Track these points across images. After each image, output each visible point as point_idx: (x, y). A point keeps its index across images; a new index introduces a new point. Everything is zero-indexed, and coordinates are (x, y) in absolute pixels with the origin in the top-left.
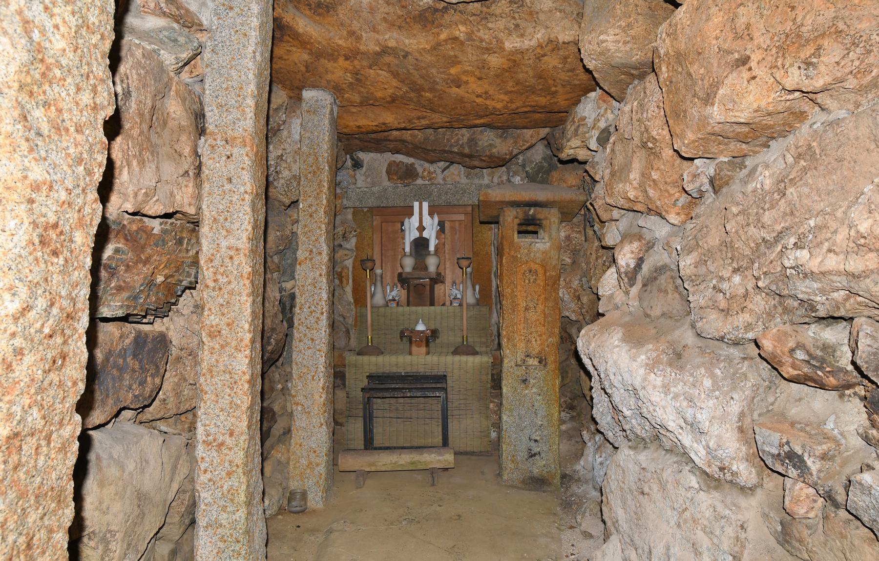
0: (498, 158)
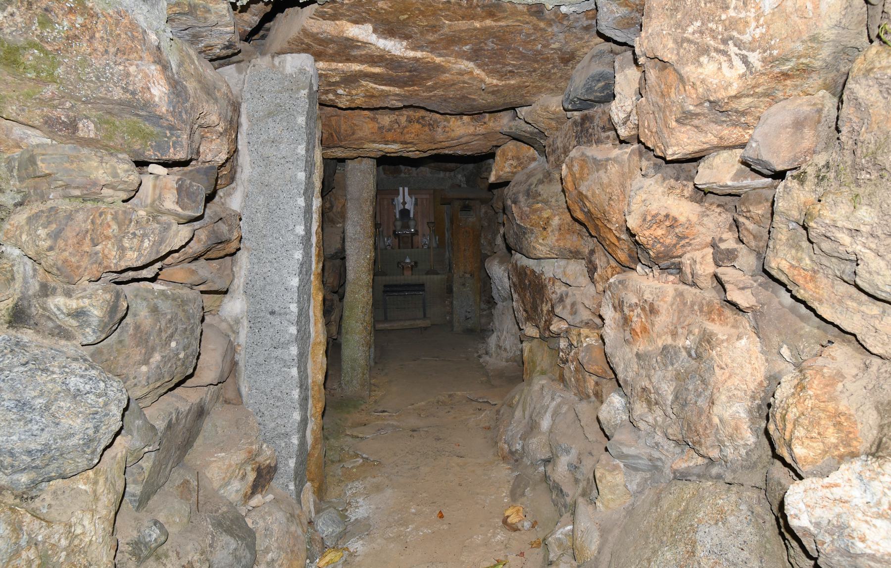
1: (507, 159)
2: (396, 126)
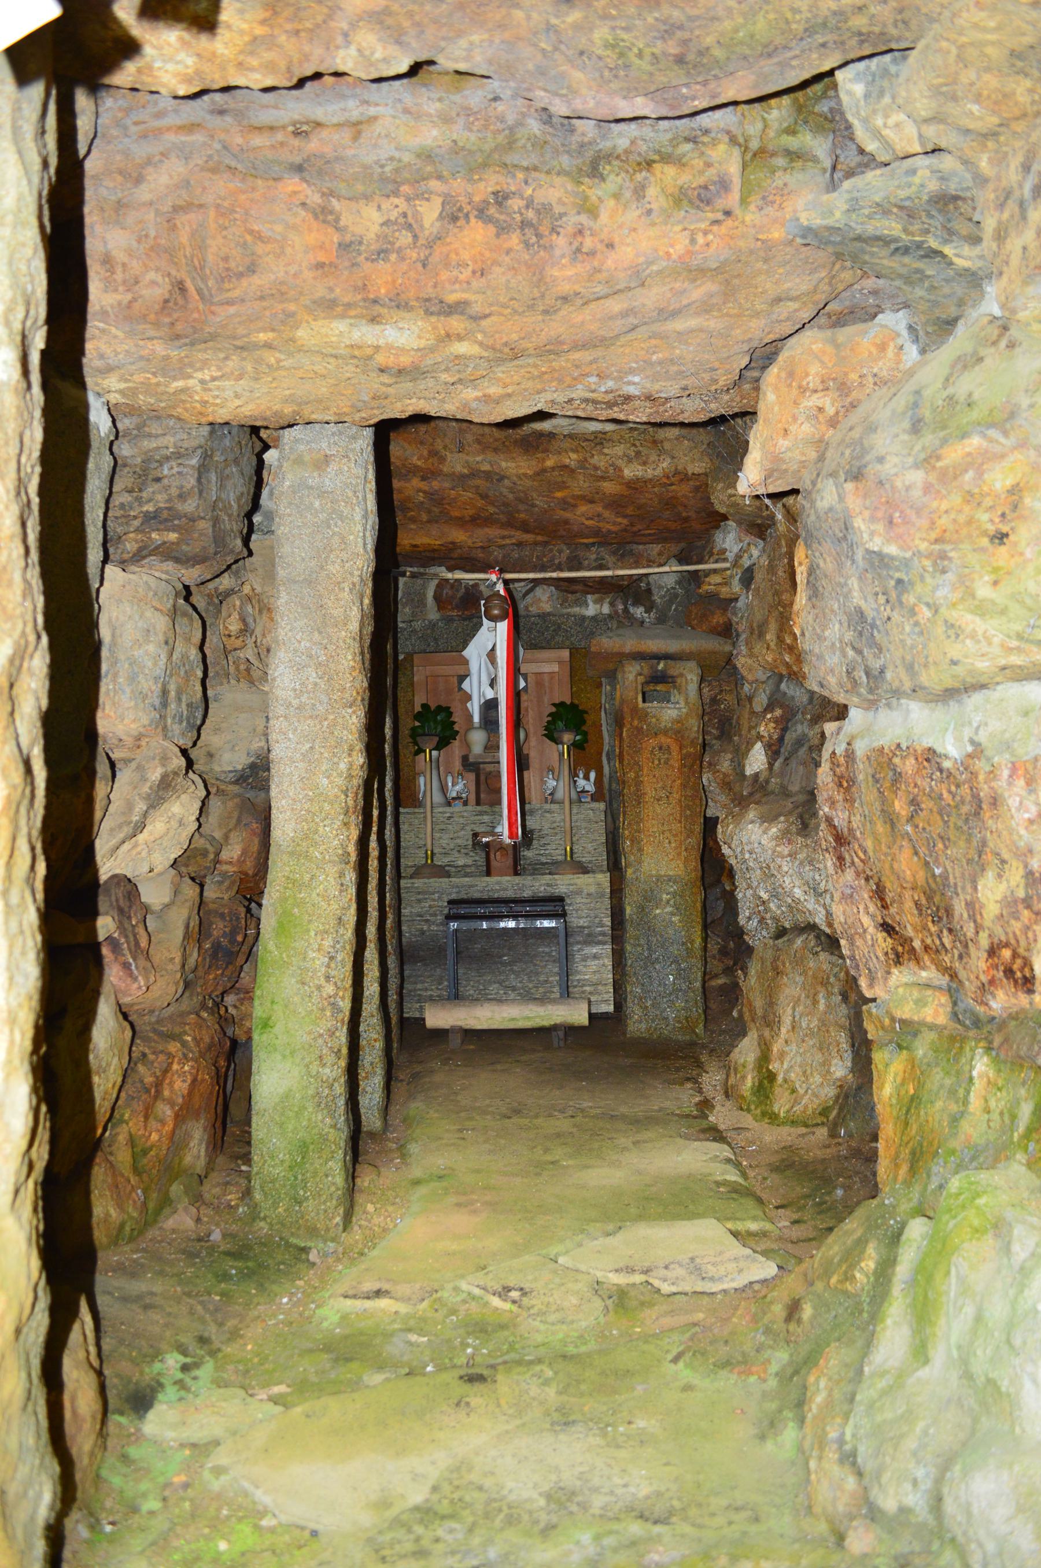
1: (803, 390)
2: (405, 238)
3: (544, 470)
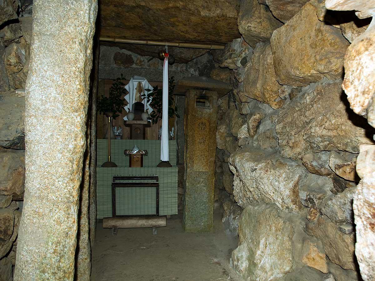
0: (184, 59)
3: (168, 8)
